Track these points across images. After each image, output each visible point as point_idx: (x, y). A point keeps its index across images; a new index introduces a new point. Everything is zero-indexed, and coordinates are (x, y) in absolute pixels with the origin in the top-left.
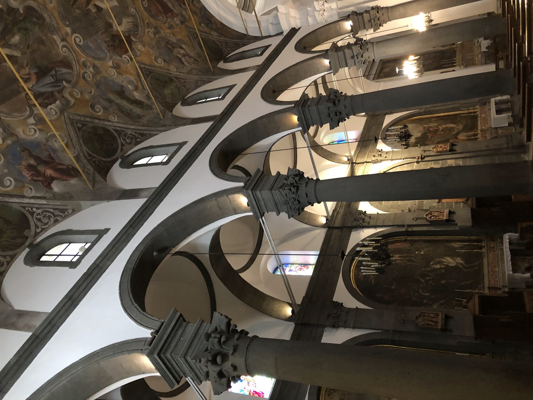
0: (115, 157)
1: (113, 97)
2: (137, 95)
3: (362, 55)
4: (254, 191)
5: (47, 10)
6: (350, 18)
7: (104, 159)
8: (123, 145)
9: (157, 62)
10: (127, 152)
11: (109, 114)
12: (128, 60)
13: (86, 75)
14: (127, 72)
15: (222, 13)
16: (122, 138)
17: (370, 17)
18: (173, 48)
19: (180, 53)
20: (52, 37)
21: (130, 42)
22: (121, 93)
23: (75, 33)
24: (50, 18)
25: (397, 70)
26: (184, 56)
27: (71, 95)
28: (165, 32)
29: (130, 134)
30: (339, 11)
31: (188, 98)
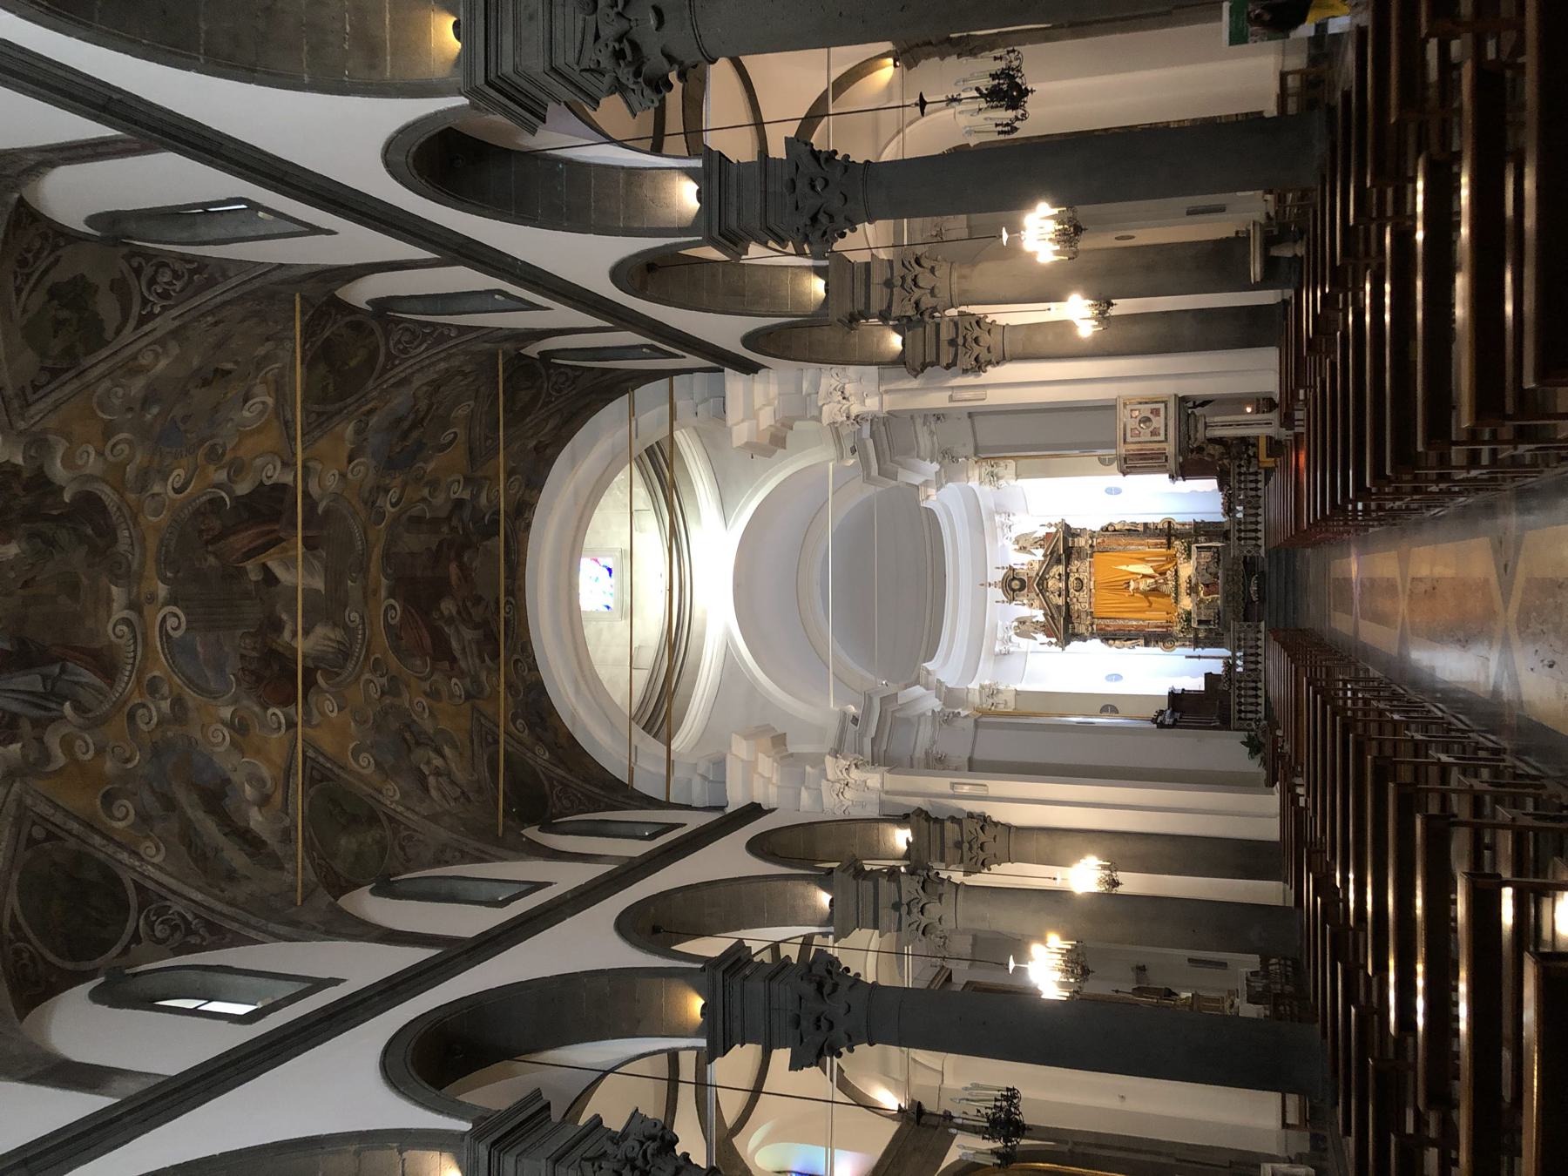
0: (91, 967)
1: (183, 796)
2: (256, 819)
3: (922, 908)
4: (500, 1152)
5: (136, 524)
6: (909, 822)
7: (51, 958)
8: (136, 938)
9: (357, 761)
10: (138, 965)
11: (148, 837)
12: (280, 723)
13: (140, 712)
14: (258, 752)
15: (582, 713)
16: (147, 917)
17: (962, 835)
18: (418, 744)
19: (428, 763)
20: (109, 589)
21: (310, 683)
22: (215, 797)
23: (176, 604)
24: (132, 544)
25: (1012, 965)
26: (437, 773)
27: (67, 744)
28: (414, 700)
29: (179, 913)
30: (884, 797)
31: (396, 882)
